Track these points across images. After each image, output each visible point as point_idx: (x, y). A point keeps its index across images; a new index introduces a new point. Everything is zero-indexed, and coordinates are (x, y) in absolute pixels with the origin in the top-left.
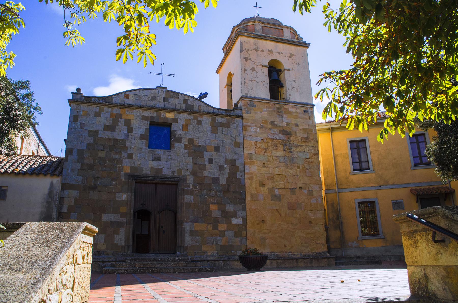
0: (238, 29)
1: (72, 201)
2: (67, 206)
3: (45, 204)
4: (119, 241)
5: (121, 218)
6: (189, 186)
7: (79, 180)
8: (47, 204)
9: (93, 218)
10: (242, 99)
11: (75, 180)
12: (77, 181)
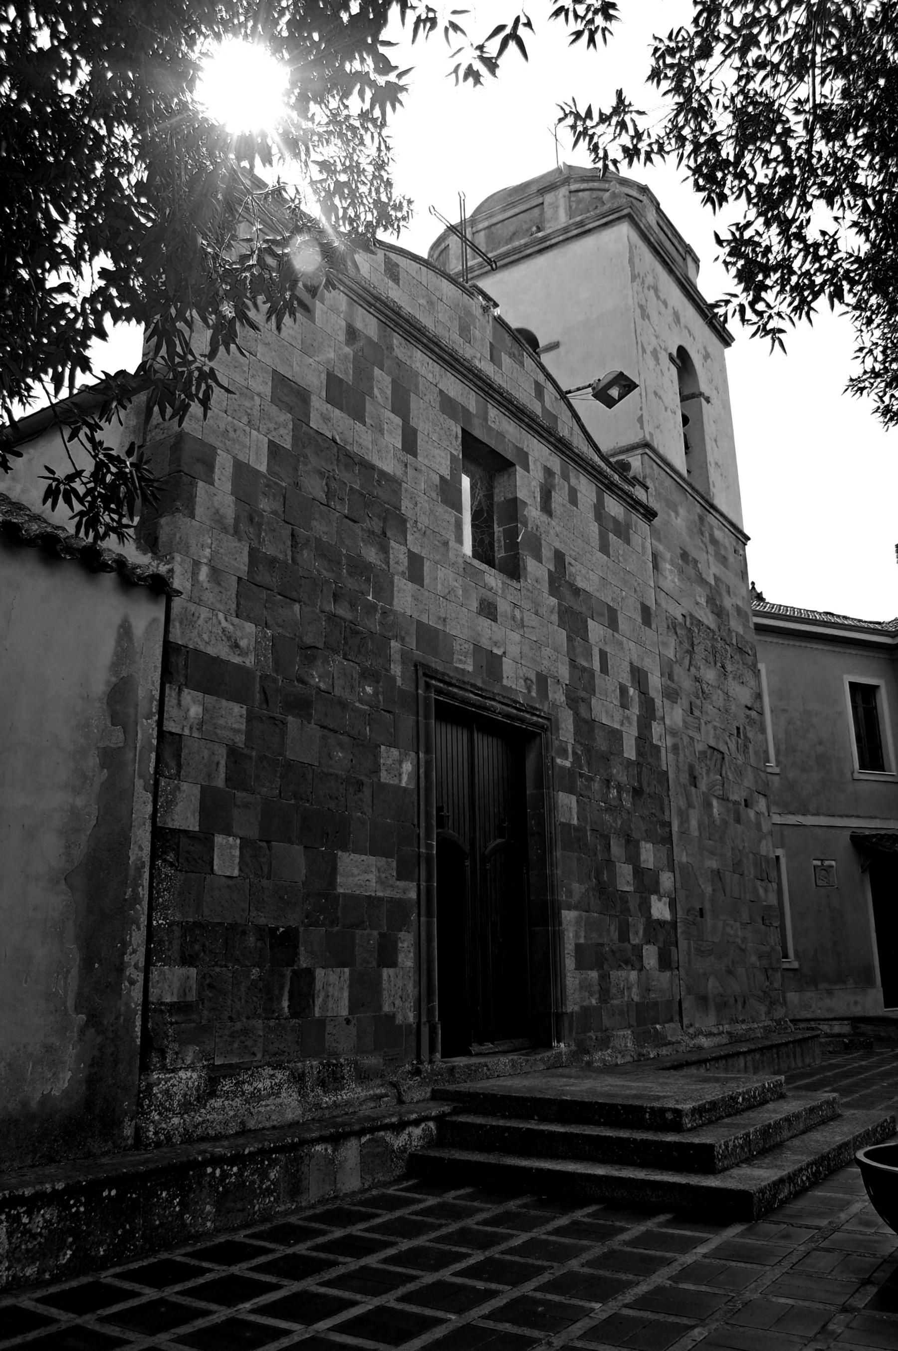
0: (583, 190)
1: (218, 764)
2: (196, 790)
3: (92, 761)
4: (398, 1002)
5: (399, 879)
6: (563, 753)
7: (243, 643)
8: (102, 767)
9: (304, 871)
10: (647, 451)
11: (229, 638)
12: (237, 646)
